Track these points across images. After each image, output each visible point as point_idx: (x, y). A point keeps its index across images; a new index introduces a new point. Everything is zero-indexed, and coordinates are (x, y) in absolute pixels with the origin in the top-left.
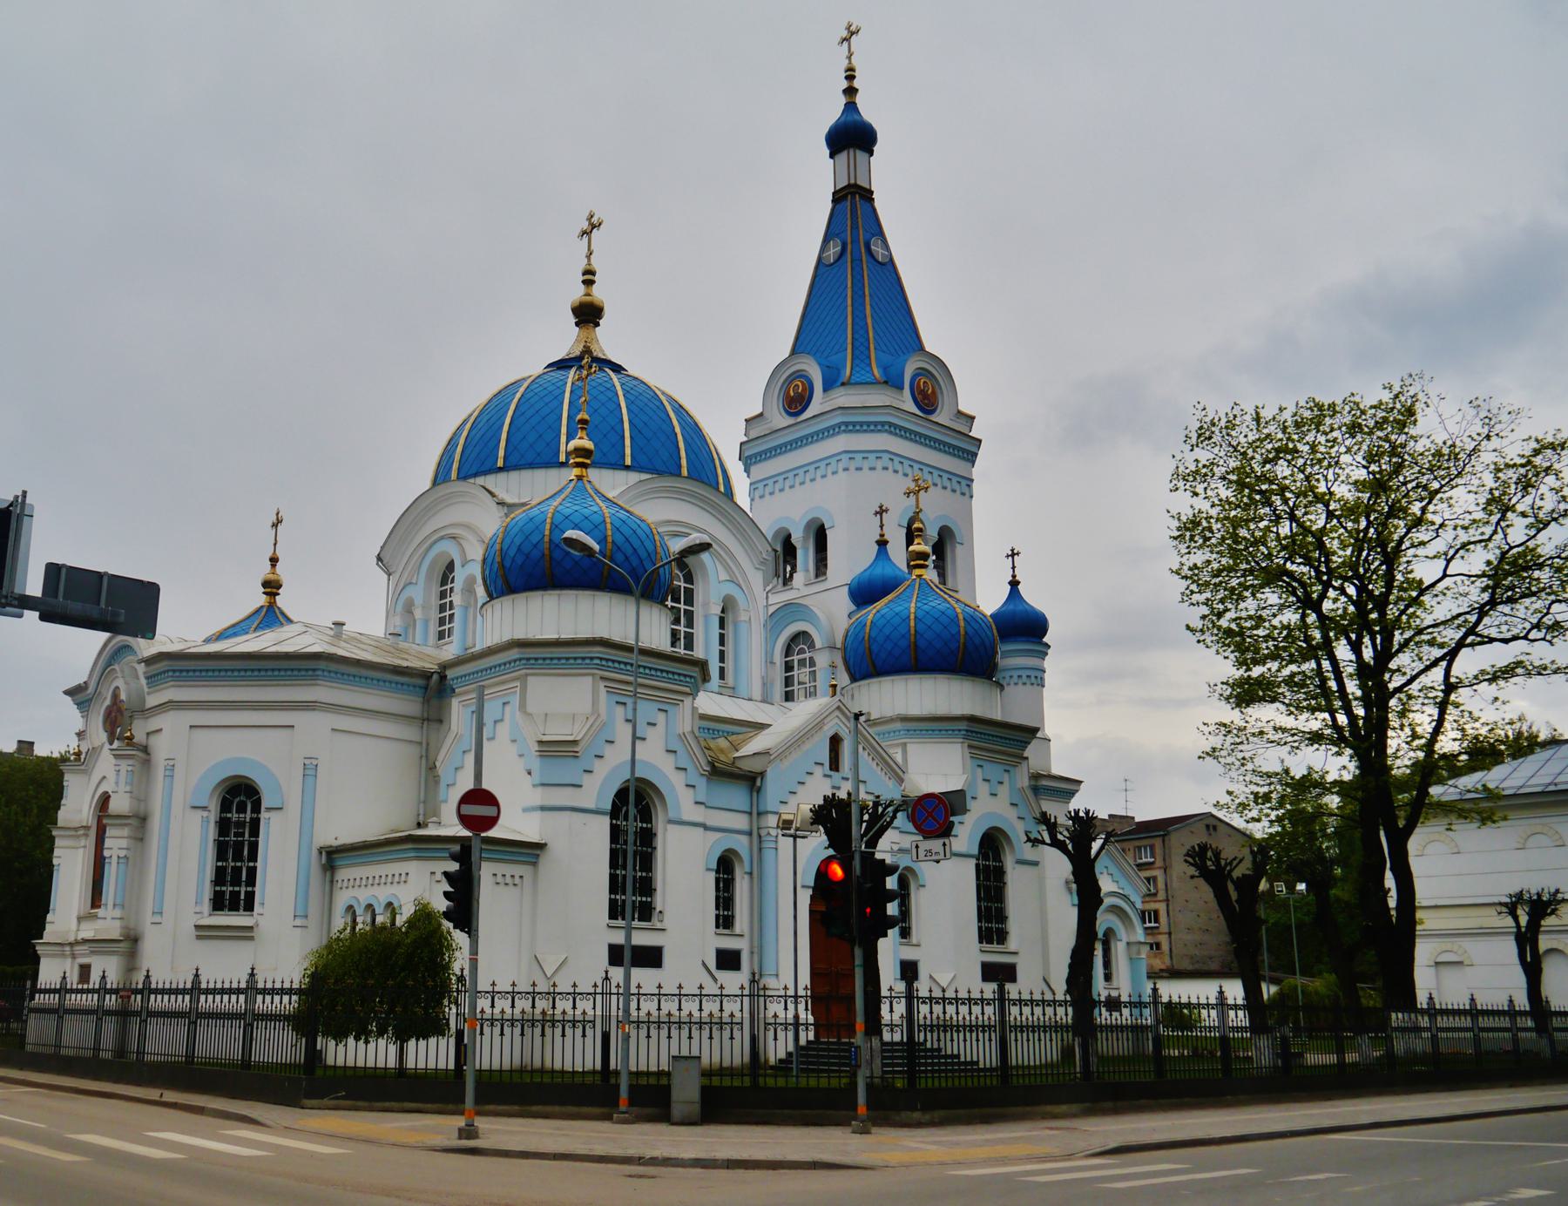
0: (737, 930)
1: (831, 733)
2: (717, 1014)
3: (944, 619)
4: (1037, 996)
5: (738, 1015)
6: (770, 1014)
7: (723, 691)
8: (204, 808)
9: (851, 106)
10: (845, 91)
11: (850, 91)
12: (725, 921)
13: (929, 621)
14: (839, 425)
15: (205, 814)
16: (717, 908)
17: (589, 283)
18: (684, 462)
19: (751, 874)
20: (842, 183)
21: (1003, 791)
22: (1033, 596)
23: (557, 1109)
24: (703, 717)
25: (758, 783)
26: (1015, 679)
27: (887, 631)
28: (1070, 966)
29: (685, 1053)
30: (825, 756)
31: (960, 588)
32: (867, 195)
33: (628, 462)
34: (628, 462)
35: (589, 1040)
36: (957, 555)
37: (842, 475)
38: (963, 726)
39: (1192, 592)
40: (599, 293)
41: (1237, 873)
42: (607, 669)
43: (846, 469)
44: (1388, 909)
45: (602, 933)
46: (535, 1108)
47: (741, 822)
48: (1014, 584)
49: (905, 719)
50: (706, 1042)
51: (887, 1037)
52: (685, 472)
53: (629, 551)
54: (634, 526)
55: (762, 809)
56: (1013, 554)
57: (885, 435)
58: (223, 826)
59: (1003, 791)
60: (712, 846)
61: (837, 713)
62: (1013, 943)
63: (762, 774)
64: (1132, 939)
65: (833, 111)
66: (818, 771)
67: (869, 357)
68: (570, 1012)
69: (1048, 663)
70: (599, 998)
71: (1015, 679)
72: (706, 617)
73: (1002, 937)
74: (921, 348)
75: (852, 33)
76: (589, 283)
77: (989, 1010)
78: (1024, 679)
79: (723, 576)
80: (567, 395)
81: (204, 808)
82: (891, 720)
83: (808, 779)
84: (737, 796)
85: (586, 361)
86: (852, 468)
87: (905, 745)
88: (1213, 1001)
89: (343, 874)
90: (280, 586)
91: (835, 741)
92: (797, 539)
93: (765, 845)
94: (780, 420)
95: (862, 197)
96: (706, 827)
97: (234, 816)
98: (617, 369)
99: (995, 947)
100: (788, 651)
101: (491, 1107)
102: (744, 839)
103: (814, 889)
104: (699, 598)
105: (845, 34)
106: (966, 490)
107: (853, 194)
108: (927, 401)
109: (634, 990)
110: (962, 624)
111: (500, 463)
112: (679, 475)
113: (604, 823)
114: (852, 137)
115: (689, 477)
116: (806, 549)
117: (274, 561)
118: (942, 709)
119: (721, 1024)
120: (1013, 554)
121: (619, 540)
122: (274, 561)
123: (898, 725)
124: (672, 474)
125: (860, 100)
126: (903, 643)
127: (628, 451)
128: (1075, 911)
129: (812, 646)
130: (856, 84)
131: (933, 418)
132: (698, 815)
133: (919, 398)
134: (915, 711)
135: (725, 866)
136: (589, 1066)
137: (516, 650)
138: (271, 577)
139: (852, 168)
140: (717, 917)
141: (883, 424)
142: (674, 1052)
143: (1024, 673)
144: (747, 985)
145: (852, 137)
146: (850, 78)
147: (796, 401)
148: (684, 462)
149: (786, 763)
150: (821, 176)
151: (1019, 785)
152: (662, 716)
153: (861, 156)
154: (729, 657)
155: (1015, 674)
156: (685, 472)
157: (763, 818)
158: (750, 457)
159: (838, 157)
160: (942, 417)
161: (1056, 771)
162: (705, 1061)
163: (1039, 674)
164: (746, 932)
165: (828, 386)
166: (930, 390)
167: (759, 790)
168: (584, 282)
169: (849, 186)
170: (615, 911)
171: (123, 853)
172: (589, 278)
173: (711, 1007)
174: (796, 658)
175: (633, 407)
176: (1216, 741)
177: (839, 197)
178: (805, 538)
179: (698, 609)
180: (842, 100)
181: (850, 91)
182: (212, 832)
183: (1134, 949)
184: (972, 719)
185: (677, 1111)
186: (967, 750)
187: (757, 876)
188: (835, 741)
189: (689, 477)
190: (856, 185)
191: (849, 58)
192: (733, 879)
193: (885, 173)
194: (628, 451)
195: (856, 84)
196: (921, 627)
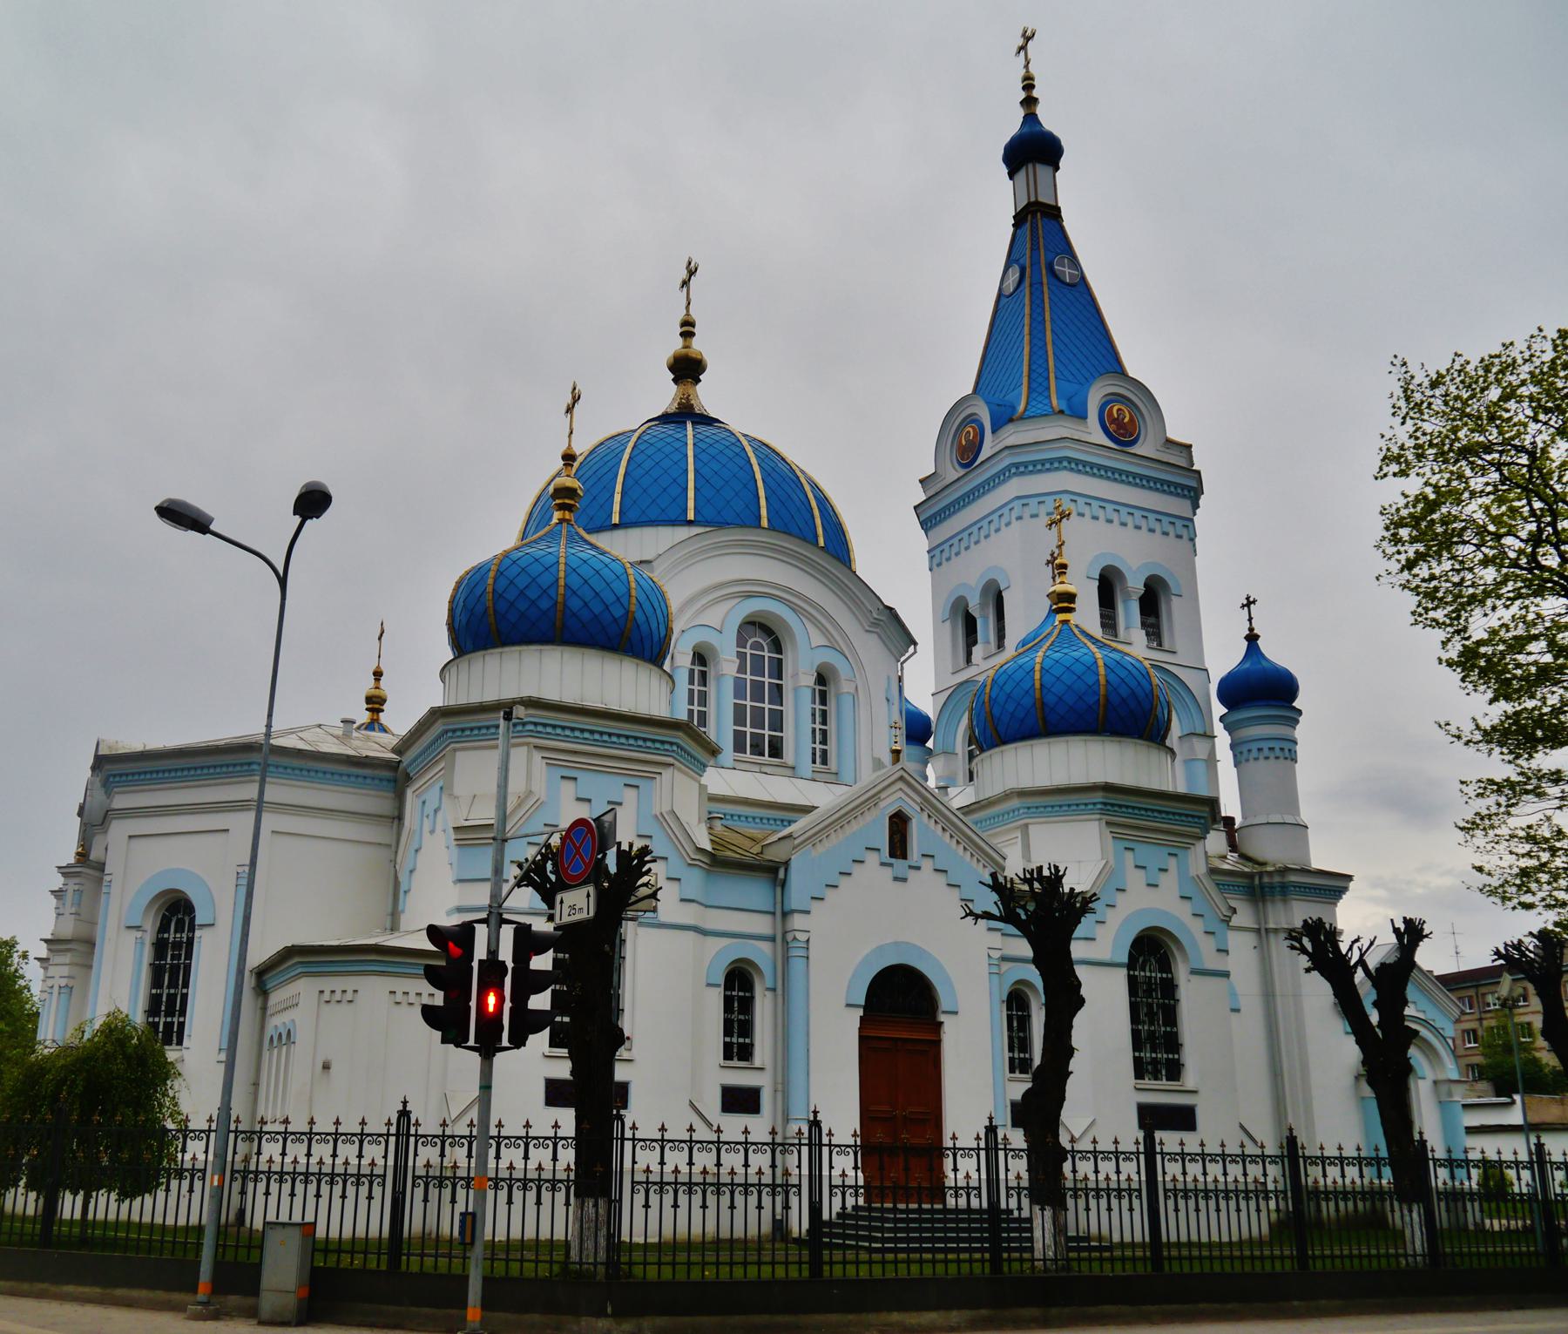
0: (757, 1062)
1: (892, 810)
2: (712, 1169)
3: (1079, 669)
4: (1233, 1149)
5: (975, 1175)
6: (421, 1162)
7: (817, 776)
8: (138, 928)
9: (1031, 118)
11: (1029, 102)
12: (738, 1048)
13: (1057, 671)
14: (1008, 468)
15: (139, 934)
16: (1011, 1049)
17: (687, 335)
18: (764, 512)
19: (774, 990)
21: (1169, 882)
22: (1276, 652)
23: (143, 1294)
24: (713, 799)
25: (781, 874)
26: (1255, 753)
27: (522, 582)
28: (1061, 1098)
29: (284, 1218)
30: (883, 842)
31: (1178, 648)
32: (1054, 213)
33: (691, 516)
34: (691, 516)
35: (376, 1203)
36: (1174, 611)
37: (1015, 524)
38: (1098, 797)
39: (1427, 610)
40: (698, 345)
41: (1372, 962)
42: (548, 736)
43: (1019, 518)
44: (1539, 994)
45: (719, 1075)
46: (119, 1292)
47: (762, 925)
48: (1252, 638)
49: (1022, 793)
50: (697, 1213)
51: (951, 1202)
52: (765, 523)
53: (588, 595)
54: (598, 566)
55: (786, 909)
56: (1249, 603)
57: (1065, 473)
58: (160, 947)
59: (1169, 882)
60: (717, 956)
61: (900, 785)
62: (1190, 1079)
63: (787, 864)
64: (1441, 1077)
65: (1011, 123)
66: (872, 859)
67: (1048, 388)
68: (684, 1169)
69: (1300, 732)
70: (213, 1135)
71: (1255, 753)
72: (796, 689)
73: (1174, 1070)
74: (1118, 369)
75: (1028, 37)
76: (687, 335)
77: (1129, 1168)
78: (1266, 752)
79: (817, 639)
80: (691, 460)
81: (138, 928)
82: (1007, 796)
83: (856, 869)
84: (755, 892)
85: (685, 414)
86: (1026, 515)
87: (1026, 825)
88: (1523, 1156)
89: (276, 998)
90: (703, 370)
91: (899, 824)
92: (974, 610)
93: (793, 952)
94: (952, 473)
95: (1044, 214)
96: (704, 932)
97: (171, 936)
99: (1164, 1083)
101: (70, 1288)
102: (766, 947)
103: (866, 1008)
104: (788, 669)
105: (1021, 42)
106: (1184, 532)
107: (1034, 214)
108: (1122, 432)
109: (493, 1132)
110: (1102, 671)
111: (616, 519)
112: (759, 526)
113: (1122, 974)
114: (1033, 151)
115: (772, 528)
116: (986, 618)
117: (378, 674)
118: (1079, 778)
119: (718, 1186)
120: (1249, 603)
121: (575, 582)
122: (378, 674)
123: (1015, 803)
124: (743, 525)
125: (1040, 111)
126: (1027, 702)
127: (691, 504)
128: (1352, 1038)
130: (1035, 93)
131: (1133, 450)
132: (688, 915)
133: (1112, 428)
134: (1043, 781)
135: (739, 983)
136: (1138, 1238)
138: (377, 692)
140: (1011, 1060)
141: (1060, 460)
142: (271, 1217)
143: (1265, 745)
144: (394, 1121)
145: (1033, 151)
146: (1028, 84)
147: (968, 454)
148: (764, 512)
149: (820, 849)
150: (998, 199)
151: (1193, 873)
152: (632, 793)
153: (1043, 171)
154: (832, 737)
155: (1254, 746)
156: (765, 523)
157: (790, 918)
158: (929, 519)
159: (1016, 177)
160: (1146, 447)
161: (1316, 864)
162: (320, 1232)
163: (1286, 745)
164: (768, 1065)
165: (995, 430)
166: (1129, 418)
167: (783, 884)
168: (682, 334)
169: (1029, 204)
170: (1140, 1070)
171: (63, 982)
172: (688, 329)
173: (704, 1159)
175: (704, 457)
176: (1481, 805)
177: (1020, 219)
178: (983, 605)
179: (787, 683)
180: (1020, 113)
181: (1029, 102)
182: (147, 955)
183: (1444, 1088)
184: (1108, 788)
185: (268, 1302)
186: (1107, 831)
187: (782, 991)
188: (899, 824)
189: (772, 528)
190: (1037, 203)
191: (1026, 66)
192: (752, 998)
193: (1074, 190)
194: (691, 504)
195: (1035, 93)
196: (1048, 679)
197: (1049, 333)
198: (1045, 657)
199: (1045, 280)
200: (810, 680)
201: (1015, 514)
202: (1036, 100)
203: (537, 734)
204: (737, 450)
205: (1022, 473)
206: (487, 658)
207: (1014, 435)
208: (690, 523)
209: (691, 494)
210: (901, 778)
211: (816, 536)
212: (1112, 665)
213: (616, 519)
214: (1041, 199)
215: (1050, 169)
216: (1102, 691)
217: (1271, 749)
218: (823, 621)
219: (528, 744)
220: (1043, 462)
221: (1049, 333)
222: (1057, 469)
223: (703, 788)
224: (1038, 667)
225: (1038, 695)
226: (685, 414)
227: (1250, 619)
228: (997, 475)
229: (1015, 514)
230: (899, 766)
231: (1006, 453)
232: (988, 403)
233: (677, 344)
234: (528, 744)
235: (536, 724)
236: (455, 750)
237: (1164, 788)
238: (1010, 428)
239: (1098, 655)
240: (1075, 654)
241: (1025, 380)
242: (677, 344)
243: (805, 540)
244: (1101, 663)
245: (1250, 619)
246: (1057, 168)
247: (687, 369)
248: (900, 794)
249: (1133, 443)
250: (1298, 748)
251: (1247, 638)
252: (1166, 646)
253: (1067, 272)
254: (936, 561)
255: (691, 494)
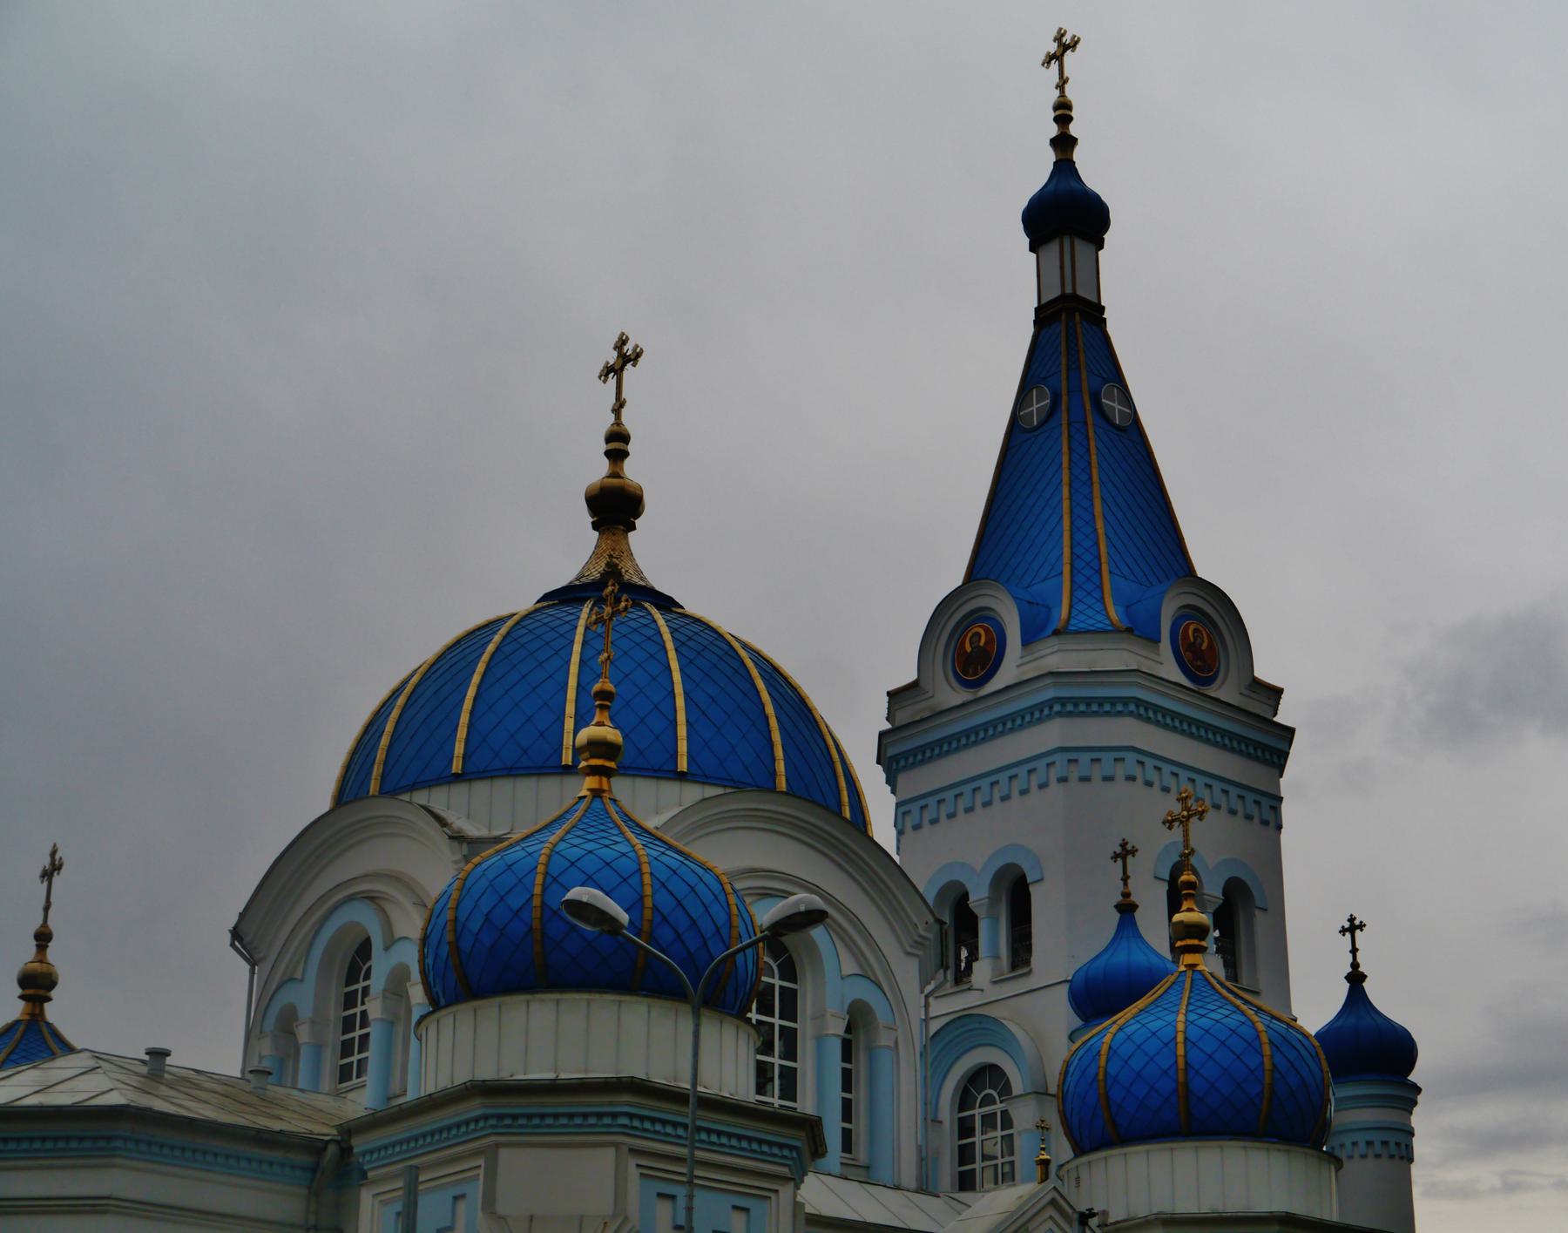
9: (1065, 167)
10: (1055, 142)
11: (1064, 143)
14: (1050, 704)
18: (781, 767)
20: (1053, 293)
33: (683, 765)
34: (683, 765)
37: (1054, 787)
40: (632, 470)
43: (1063, 780)
48: (1356, 978)
52: (782, 784)
61: (1051, 1211)
65: (1038, 170)
67: (1100, 587)
72: (820, 1039)
78: (1378, 1148)
79: (850, 967)
80: (577, 648)
85: (611, 590)
98: (666, 604)
100: (964, 1099)
104: (806, 1006)
105: (1053, 48)
110: (1267, 1050)
111: (457, 766)
112: (773, 789)
114: (1066, 217)
116: (995, 919)
125: (1079, 156)
127: (683, 747)
129: (1006, 1090)
131: (1212, 691)
133: (1187, 656)
137: (477, 1101)
139: (1068, 269)
141: (1126, 701)
145: (1066, 217)
148: (781, 767)
150: (1015, 282)
153: (1082, 248)
156: (782, 784)
159: (1042, 251)
160: (1226, 690)
165: (1028, 639)
168: (608, 454)
169: (1063, 297)
172: (617, 444)
174: (978, 1112)
177: (1045, 316)
178: (993, 900)
180: (1049, 157)
181: (1064, 143)
190: (1074, 297)
193: (1123, 277)
197: (1098, 502)
198: (554, 851)
199: (1090, 420)
200: (837, 1027)
201: (1054, 773)
202: (1074, 141)
203: (627, 1131)
204: (650, 633)
205: (1070, 714)
206: (534, 1006)
207: (1057, 656)
208: (681, 777)
209: (682, 731)
210: (1053, 1202)
211: (840, 804)
212: (663, 875)
213: (457, 766)
214: (1081, 292)
215: (1093, 248)
216: (1267, 1079)
217: (1385, 1143)
218: (863, 945)
219: (616, 1145)
220: (1101, 701)
221: (1098, 502)
222: (1120, 714)
223: (797, 1206)
224: (1180, 1038)
225: (1181, 1079)
226: (611, 590)
227: (1125, 879)
228: (1031, 710)
229: (1054, 773)
230: (1049, 1185)
231: (1049, 681)
232: (1015, 598)
233: (599, 469)
234: (616, 1145)
235: (631, 1116)
236: (498, 1145)
237: (1326, 1217)
238: (1052, 644)
239: (1261, 1027)
240: (607, 854)
241: (1066, 569)
242: (599, 469)
243: (826, 808)
244: (1264, 1038)
245: (1354, 951)
246: (1100, 245)
247: (615, 508)
248: (1049, 1224)
249: (1209, 681)
250: (1415, 1140)
251: (1119, 907)
252: (1245, 980)
253: (1112, 404)
254: (909, 823)
255: (682, 731)
